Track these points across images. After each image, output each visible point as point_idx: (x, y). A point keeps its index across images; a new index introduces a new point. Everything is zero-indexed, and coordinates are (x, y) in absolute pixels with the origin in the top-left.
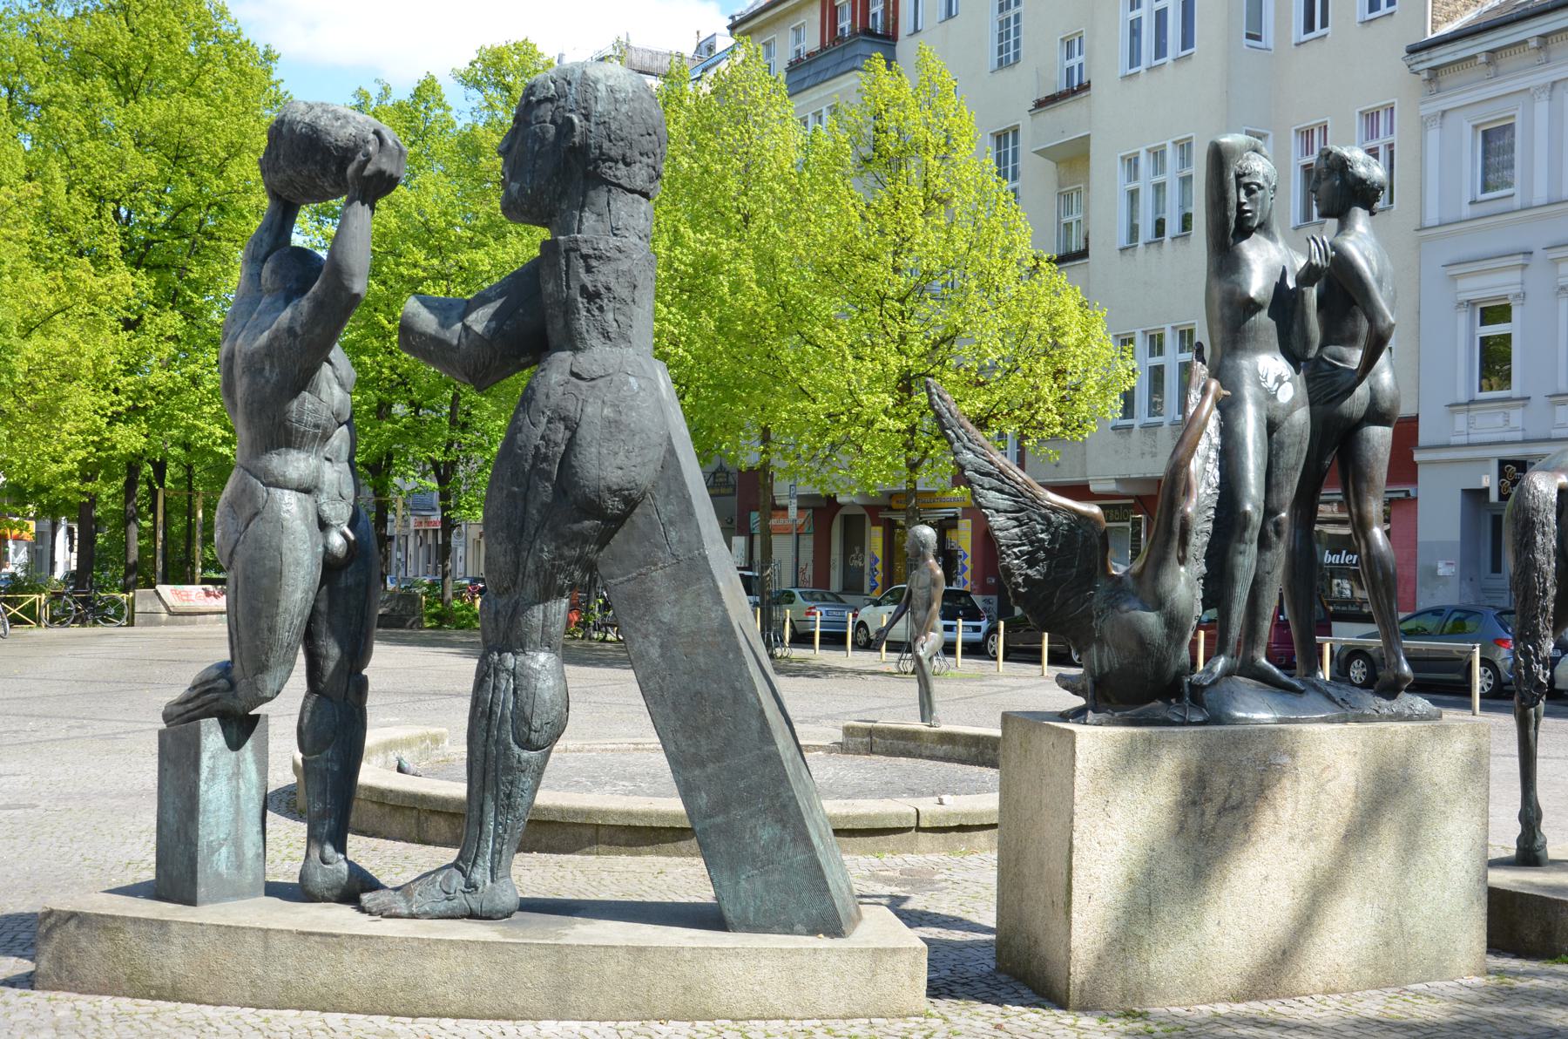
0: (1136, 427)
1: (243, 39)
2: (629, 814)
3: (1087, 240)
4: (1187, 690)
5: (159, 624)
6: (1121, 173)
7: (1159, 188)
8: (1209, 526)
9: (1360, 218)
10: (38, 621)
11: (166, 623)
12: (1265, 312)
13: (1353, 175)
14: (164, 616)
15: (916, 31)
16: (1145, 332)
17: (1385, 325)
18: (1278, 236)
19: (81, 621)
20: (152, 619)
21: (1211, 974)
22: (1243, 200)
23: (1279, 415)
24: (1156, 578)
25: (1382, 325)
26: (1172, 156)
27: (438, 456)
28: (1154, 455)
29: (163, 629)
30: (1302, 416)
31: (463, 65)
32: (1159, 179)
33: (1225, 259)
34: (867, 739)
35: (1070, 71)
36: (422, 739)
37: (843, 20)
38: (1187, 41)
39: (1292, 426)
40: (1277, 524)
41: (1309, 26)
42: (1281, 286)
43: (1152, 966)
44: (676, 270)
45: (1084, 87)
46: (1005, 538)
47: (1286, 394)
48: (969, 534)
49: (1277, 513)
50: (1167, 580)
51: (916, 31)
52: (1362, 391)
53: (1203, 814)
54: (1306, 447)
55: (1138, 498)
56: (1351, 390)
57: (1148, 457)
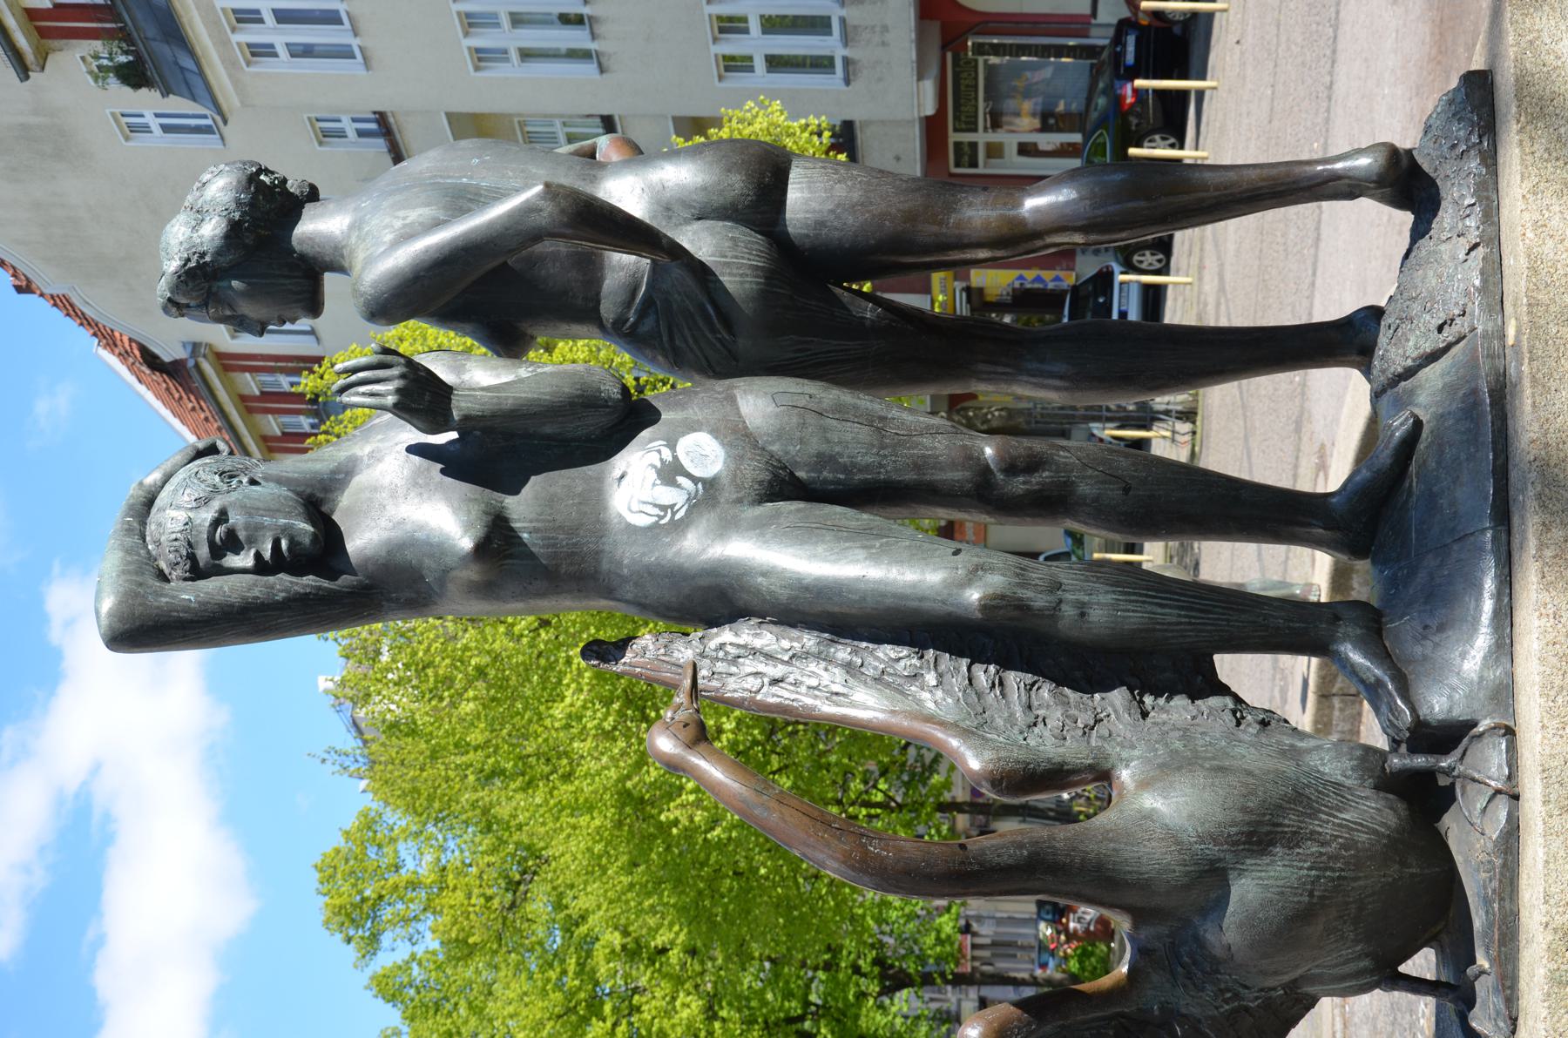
0: (846, 52)
3: (588, 116)
4: (1420, 761)
8: (1013, 678)
9: (317, 227)
12: (510, 501)
13: (219, 253)
16: (715, 40)
17: (548, 208)
22: (245, 560)
23: (754, 471)
25: (548, 214)
27: (874, 988)
28: (885, 29)
30: (758, 403)
31: (351, 952)
34: (1336, 702)
35: (361, 134)
37: (300, 426)
39: (780, 435)
40: (1012, 468)
42: (454, 464)
44: (615, 728)
45: (381, 118)
49: (985, 470)
50: (1153, 856)
52: (701, 241)
55: (945, 47)
56: (701, 272)
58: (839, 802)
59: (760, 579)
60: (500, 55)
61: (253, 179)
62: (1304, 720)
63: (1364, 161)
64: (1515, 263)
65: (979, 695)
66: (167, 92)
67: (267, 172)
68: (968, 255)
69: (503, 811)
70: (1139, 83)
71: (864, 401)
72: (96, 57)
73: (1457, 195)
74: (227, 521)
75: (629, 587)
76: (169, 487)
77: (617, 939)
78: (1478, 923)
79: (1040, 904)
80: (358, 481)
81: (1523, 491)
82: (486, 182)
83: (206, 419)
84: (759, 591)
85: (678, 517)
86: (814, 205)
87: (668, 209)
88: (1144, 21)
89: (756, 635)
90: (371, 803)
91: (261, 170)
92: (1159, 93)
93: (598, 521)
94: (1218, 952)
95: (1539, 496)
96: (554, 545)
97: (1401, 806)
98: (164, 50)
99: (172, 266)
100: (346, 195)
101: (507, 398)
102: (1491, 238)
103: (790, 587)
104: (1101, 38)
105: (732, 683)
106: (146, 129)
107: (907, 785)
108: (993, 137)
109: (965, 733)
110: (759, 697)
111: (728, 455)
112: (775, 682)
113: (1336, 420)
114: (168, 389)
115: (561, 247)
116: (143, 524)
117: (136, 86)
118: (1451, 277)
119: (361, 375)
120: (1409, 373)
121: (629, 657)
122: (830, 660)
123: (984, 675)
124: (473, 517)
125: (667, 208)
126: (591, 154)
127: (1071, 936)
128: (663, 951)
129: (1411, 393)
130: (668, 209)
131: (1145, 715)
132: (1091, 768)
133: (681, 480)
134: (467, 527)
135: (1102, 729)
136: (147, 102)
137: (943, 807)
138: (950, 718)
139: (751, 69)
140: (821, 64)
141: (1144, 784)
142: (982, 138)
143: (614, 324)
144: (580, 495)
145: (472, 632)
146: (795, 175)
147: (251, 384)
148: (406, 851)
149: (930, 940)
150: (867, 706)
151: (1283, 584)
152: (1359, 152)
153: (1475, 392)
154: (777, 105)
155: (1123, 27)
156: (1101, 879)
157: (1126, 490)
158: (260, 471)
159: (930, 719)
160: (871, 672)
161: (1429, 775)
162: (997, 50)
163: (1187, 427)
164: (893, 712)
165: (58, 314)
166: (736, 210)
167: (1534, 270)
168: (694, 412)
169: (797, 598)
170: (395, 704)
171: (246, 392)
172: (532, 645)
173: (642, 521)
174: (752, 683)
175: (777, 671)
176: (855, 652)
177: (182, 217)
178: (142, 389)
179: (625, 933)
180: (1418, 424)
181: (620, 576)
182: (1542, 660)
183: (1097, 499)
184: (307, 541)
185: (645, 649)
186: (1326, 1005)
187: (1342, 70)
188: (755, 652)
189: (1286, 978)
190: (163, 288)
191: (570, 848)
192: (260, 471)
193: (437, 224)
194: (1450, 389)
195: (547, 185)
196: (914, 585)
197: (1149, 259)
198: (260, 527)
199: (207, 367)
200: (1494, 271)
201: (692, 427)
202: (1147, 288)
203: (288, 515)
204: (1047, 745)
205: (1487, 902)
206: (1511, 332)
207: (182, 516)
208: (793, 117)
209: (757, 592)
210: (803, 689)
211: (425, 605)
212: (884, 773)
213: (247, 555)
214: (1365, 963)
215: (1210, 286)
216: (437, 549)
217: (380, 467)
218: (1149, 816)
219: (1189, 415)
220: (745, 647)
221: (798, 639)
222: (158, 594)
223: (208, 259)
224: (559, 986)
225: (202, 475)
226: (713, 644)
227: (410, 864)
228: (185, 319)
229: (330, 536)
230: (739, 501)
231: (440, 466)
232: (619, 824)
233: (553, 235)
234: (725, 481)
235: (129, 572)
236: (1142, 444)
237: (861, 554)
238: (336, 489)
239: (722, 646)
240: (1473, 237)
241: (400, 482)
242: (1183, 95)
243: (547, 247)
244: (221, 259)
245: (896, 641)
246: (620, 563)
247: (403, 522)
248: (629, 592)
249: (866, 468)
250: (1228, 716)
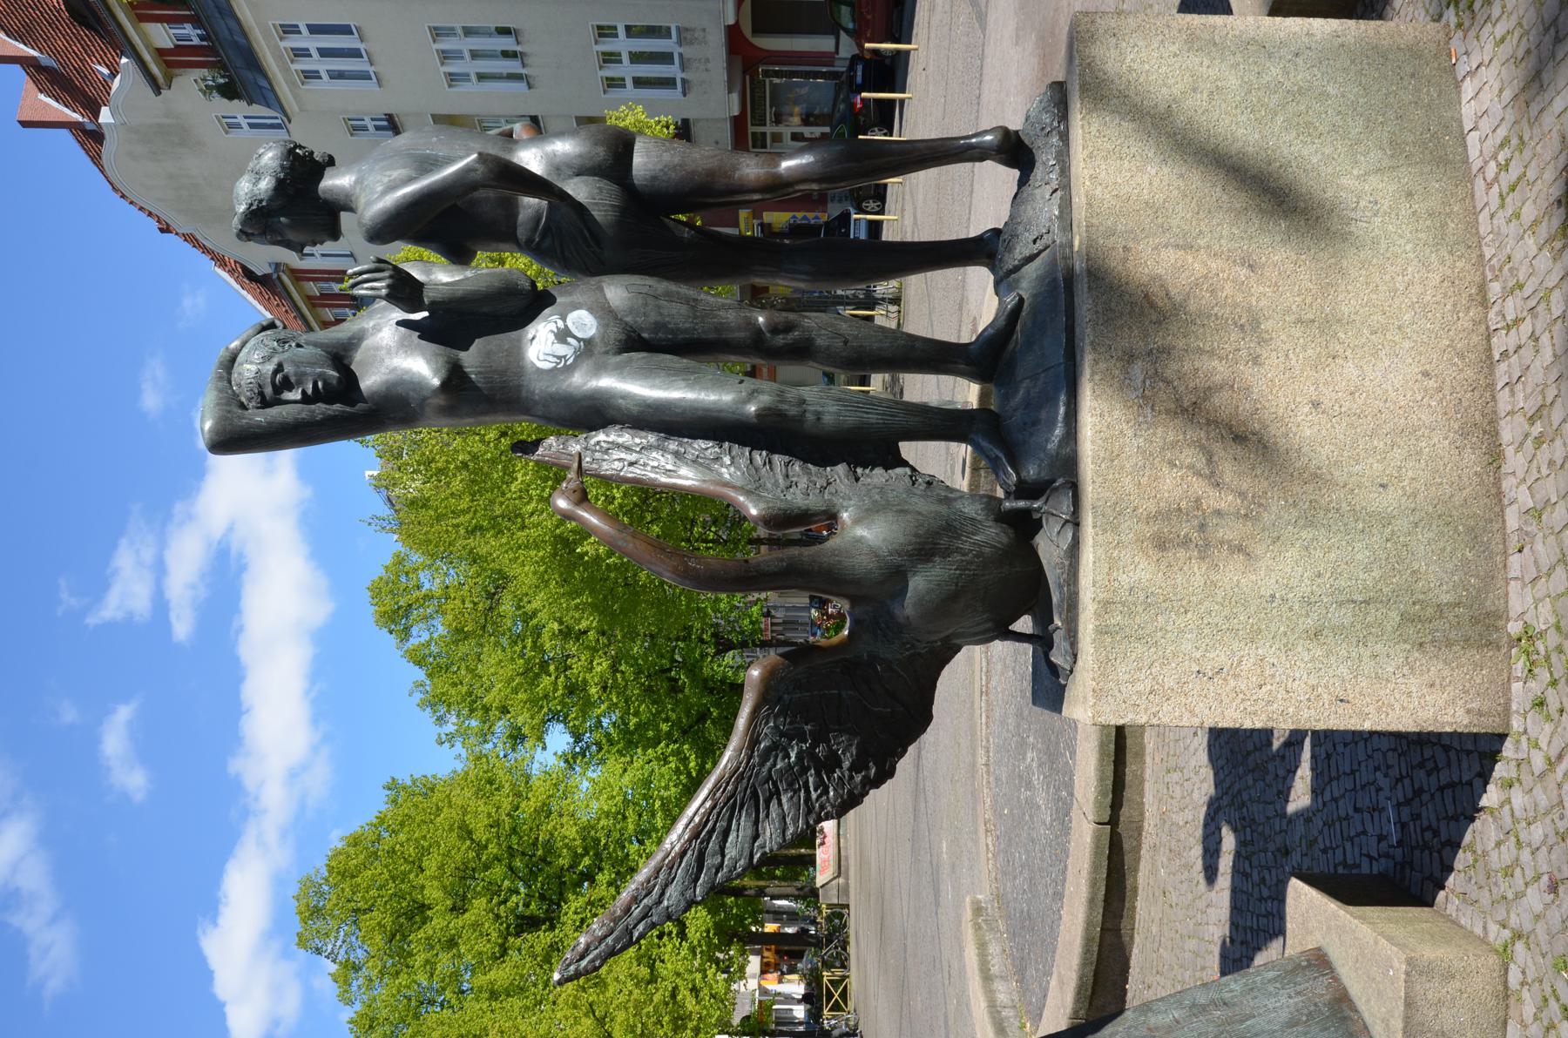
1: (375, 821)
2: (1091, 901)
4: (1021, 504)
5: (847, 884)
6: (463, 88)
7: (475, 55)
8: (777, 459)
9: (336, 182)
10: (844, 978)
11: (847, 879)
12: (463, 355)
13: (271, 200)
14: (841, 880)
15: (351, 255)
17: (481, 168)
19: (845, 944)
20: (844, 890)
21: (1457, 500)
22: (296, 395)
23: (615, 333)
24: (857, 582)
26: (447, 44)
27: (711, 651)
28: (707, 60)
29: (852, 882)
30: (617, 291)
31: (392, 640)
32: (467, 55)
33: (390, 411)
35: (378, 128)
36: (977, 927)
38: (345, 30)
39: (631, 310)
40: (775, 330)
42: (426, 332)
43: (1446, 598)
46: (795, 821)
48: (776, 214)
49: (758, 331)
50: (862, 563)
51: (351, 255)
52: (579, 190)
53: (1218, 513)
55: (744, 72)
57: (709, 66)
58: (688, 541)
60: (465, 77)
61: (291, 152)
62: (963, 484)
63: (988, 138)
64: (1079, 200)
65: (757, 470)
66: (250, 103)
67: (301, 147)
68: (747, 197)
69: (483, 551)
70: (864, 94)
71: (684, 290)
72: (204, 80)
73: (1046, 159)
76: (245, 350)
77: (556, 626)
78: (1055, 599)
79: (812, 598)
80: (366, 344)
81: (1083, 340)
82: (442, 152)
88: (868, 56)
90: (400, 547)
91: (296, 146)
92: (877, 101)
94: (901, 620)
95: (1092, 343)
97: (1010, 531)
98: (248, 75)
99: (242, 208)
100: (355, 159)
102: (1065, 186)
104: (841, 68)
106: (238, 126)
107: (730, 529)
108: (776, 129)
109: (748, 493)
112: (631, 464)
113: (982, 303)
115: (490, 194)
116: (229, 373)
117: (231, 98)
118: (1041, 210)
120: (1017, 269)
121: (541, 450)
122: (664, 450)
123: (759, 457)
125: (558, 166)
126: (510, 134)
127: (830, 617)
128: (585, 632)
129: (1017, 281)
131: (857, 479)
132: (824, 512)
134: (436, 372)
135: (831, 489)
136: (238, 109)
137: (751, 542)
138: (739, 484)
139: (624, 86)
140: (668, 83)
141: (857, 521)
142: (769, 129)
145: (459, 439)
146: (638, 147)
147: (313, 288)
148: (424, 577)
149: (746, 622)
150: (687, 477)
151: (951, 402)
152: (986, 132)
153: (1055, 280)
154: (640, 108)
155: (854, 60)
156: (824, 581)
157: (846, 342)
158: (303, 338)
159: (726, 484)
161: (1027, 513)
162: (778, 74)
163: (895, 308)
165: (188, 246)
167: (1090, 205)
168: (577, 297)
170: (415, 487)
172: (496, 447)
174: (617, 465)
175: (633, 457)
176: (680, 444)
177: (246, 177)
178: (244, 293)
179: (561, 623)
180: (1021, 300)
182: (1093, 442)
183: (828, 348)
186: (964, 649)
187: (985, 86)
188: (619, 446)
189: (943, 635)
190: (236, 223)
191: (524, 573)
192: (303, 338)
193: (410, 180)
194: (1040, 279)
196: (715, 402)
197: (872, 205)
198: (304, 374)
199: (285, 278)
200: (1066, 205)
201: (576, 307)
202: (871, 222)
203: (322, 366)
204: (798, 498)
205: (1060, 587)
206: (1076, 243)
207: (254, 368)
208: (650, 116)
209: (619, 409)
212: (715, 522)
214: (989, 625)
215: (908, 222)
216: (417, 385)
217: (380, 335)
218: (860, 540)
219: (896, 301)
222: (240, 418)
224: (522, 655)
226: (592, 442)
227: (427, 586)
228: (252, 243)
229: (349, 380)
230: (607, 353)
232: (554, 555)
233: (484, 186)
236: (870, 318)
237: (683, 384)
239: (598, 443)
240: (1054, 185)
242: (892, 102)
243: (481, 194)
245: (706, 437)
247: (395, 369)
248: (540, 410)
249: (686, 331)
250: (907, 479)
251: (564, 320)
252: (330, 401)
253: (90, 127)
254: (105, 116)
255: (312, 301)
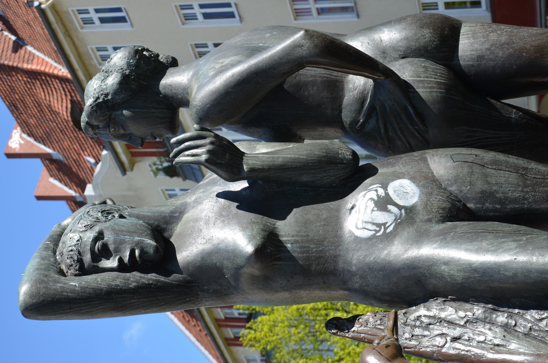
13: (116, 93)
17: (307, 44)
18: (177, 202)
22: (112, 263)
23: (438, 202)
25: (307, 47)
30: (441, 163)
37: (233, 314)
39: (456, 180)
41: (231, 15)
42: (242, 201)
47: (405, 191)
52: (405, 70)
54: (488, 156)
59: (443, 267)
67: (148, 50)
72: (155, 164)
74: (103, 238)
75: (357, 279)
80: (187, 216)
83: (200, 330)
84: (443, 276)
85: (388, 231)
86: (476, 46)
87: (384, 53)
89: (442, 310)
91: (144, 49)
93: (336, 236)
96: (308, 252)
101: (278, 158)
103: (464, 270)
105: (425, 342)
110: (444, 350)
111: (422, 193)
112: (455, 339)
114: (183, 316)
116: (56, 245)
119: (187, 144)
122: (493, 323)
124: (255, 232)
130: (384, 53)
133: (390, 207)
134: (251, 239)
143: (350, 125)
144: (325, 220)
160: (521, 329)
164: (538, 355)
166: (427, 51)
168: (399, 168)
169: (468, 278)
171: (218, 317)
173: (366, 234)
174: (439, 341)
175: (457, 332)
176: (510, 316)
181: (349, 271)
184: (151, 251)
185: (367, 322)
188: (441, 321)
193: (239, 62)
195: (307, 31)
198: (122, 242)
201: (398, 176)
207: (76, 237)
209: (441, 277)
210: (475, 343)
211: (226, 295)
213: (114, 259)
216: (232, 253)
220: (434, 317)
221: (471, 310)
223: (109, 97)
225: (91, 213)
226: (412, 317)
230: (429, 220)
231: (236, 204)
234: (420, 208)
235: (40, 269)
237: (513, 245)
238: (173, 222)
241: (210, 215)
244: (117, 97)
246: (350, 264)
251: (385, 187)
252: (145, 270)
253: (80, 199)
254: (89, 190)
255: (219, 323)
